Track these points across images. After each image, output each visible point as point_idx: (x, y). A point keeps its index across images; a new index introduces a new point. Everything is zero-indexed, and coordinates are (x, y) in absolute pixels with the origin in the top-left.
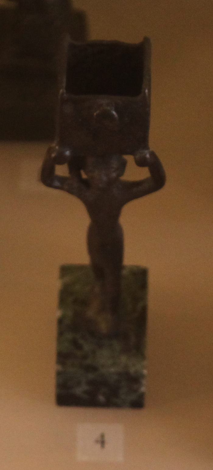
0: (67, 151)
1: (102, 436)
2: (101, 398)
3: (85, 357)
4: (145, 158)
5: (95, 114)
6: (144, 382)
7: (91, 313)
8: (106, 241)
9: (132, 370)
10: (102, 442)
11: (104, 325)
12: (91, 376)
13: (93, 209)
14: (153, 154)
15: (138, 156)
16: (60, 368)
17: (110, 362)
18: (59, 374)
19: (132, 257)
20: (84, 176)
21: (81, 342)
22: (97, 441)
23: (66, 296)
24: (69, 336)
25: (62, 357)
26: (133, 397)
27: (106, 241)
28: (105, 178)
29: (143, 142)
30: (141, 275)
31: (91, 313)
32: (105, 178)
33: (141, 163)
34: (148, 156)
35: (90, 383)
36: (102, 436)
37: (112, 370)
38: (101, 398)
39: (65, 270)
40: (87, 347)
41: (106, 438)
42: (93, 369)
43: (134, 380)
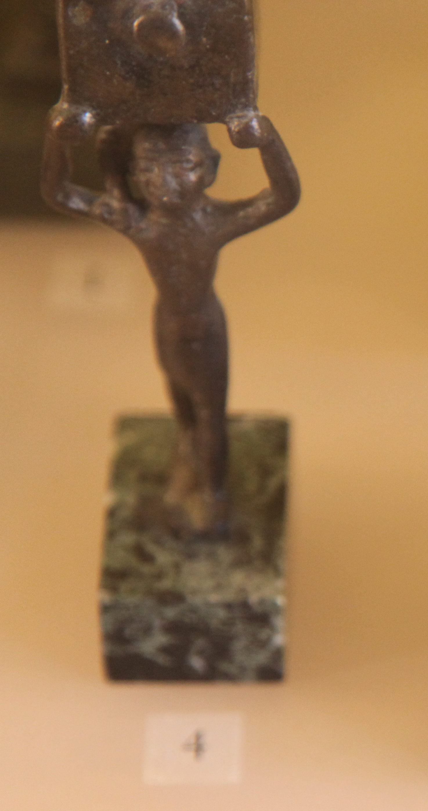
0: (85, 112)
1: (198, 737)
3: (159, 576)
4: (247, 129)
5: (136, 23)
6: (279, 622)
7: (171, 497)
8: (194, 347)
9: (254, 598)
10: (198, 747)
11: (197, 513)
12: (171, 613)
13: (159, 259)
14: (265, 121)
15: (235, 125)
16: (106, 597)
17: (208, 584)
18: (105, 609)
21: (151, 548)
22: (186, 747)
23: (123, 468)
24: (128, 538)
25: (113, 577)
26: (261, 658)
27: (194, 347)
29: (242, 92)
30: (277, 434)
31: (171, 497)
32: (173, 184)
33: (243, 139)
34: (255, 124)
35: (173, 628)
36: (198, 737)
37: (214, 598)
38: (197, 663)
39: (125, 424)
40: (163, 558)
41: (208, 740)
42: (174, 597)
43: (260, 618)
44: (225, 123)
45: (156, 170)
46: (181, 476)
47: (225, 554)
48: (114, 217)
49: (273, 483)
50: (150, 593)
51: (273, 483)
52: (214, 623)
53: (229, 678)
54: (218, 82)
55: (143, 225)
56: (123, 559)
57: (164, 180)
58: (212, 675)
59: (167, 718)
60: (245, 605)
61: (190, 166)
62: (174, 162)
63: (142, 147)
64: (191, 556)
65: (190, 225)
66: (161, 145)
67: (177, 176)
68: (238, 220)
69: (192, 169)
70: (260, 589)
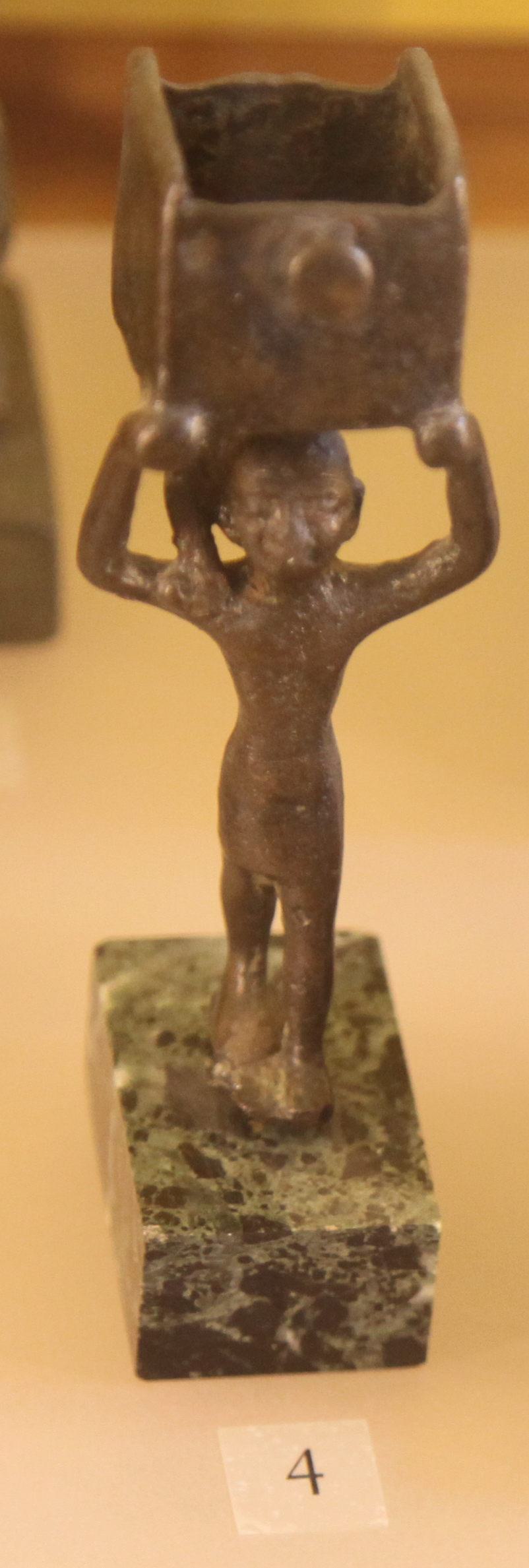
0: (192, 414)
2: (290, 1337)
3: (235, 1197)
8: (285, 824)
11: (279, 1089)
12: (259, 1255)
13: (253, 662)
14: (473, 423)
15: (427, 433)
17: (320, 1201)
19: (351, 917)
20: (229, 551)
23: (124, 1029)
26: (395, 1325)
27: (285, 824)
28: (305, 534)
29: (443, 373)
32: (305, 534)
44: (414, 428)
45: (278, 514)
46: (243, 1033)
47: (333, 1155)
48: (194, 598)
49: (377, 1041)
50: (227, 1223)
51: (377, 1041)
52: (328, 1268)
53: (339, 1362)
54: (407, 358)
55: (238, 609)
56: (167, 1171)
57: (292, 528)
58: (309, 1360)
59: (250, 1434)
60: (382, 1235)
61: (332, 504)
62: (308, 499)
63: (251, 478)
64: (280, 1162)
65: (314, 605)
66: (287, 472)
67: (312, 522)
68: (392, 593)
69: (335, 510)
70: (400, 1211)
